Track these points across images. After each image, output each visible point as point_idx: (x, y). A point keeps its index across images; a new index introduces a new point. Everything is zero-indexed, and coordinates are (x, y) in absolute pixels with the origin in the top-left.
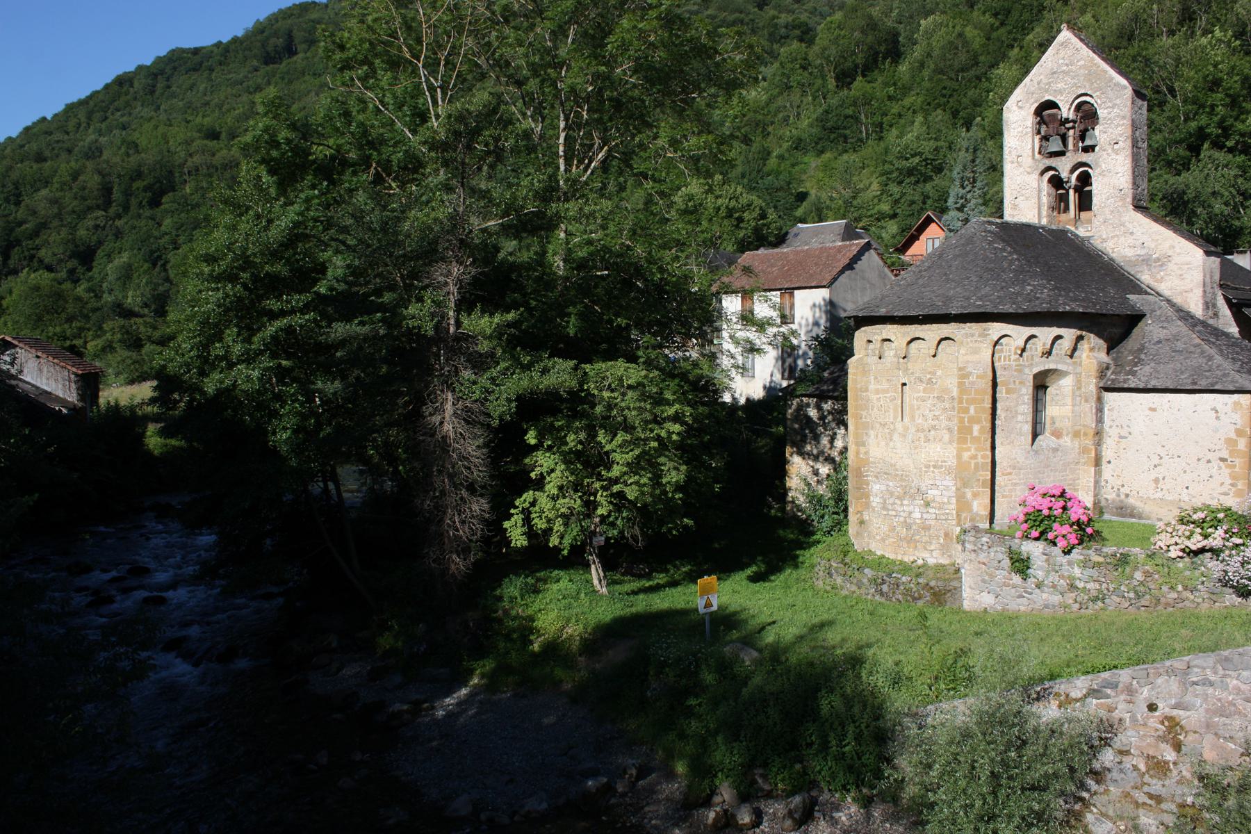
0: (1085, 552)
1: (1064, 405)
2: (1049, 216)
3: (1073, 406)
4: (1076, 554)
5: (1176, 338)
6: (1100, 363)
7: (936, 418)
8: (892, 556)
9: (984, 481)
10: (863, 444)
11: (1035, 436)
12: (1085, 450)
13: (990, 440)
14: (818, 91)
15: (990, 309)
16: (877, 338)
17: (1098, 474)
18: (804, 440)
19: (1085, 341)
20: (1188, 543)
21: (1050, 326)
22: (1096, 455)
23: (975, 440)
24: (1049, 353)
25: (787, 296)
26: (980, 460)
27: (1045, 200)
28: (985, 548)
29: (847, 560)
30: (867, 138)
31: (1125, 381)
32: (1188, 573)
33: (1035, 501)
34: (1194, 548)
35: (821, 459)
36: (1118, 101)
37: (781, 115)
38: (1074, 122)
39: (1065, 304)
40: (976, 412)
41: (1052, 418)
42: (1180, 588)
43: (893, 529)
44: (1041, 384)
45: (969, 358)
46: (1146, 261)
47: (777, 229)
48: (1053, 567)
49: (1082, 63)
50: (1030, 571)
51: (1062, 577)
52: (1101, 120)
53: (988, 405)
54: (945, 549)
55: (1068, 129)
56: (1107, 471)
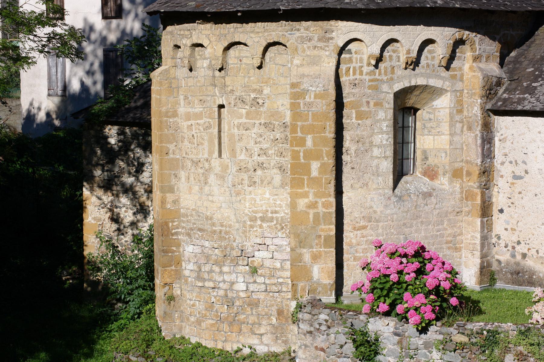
0: (445, 329)
1: (439, 134)
3: (451, 135)
4: (434, 333)
6: (487, 78)
7: (264, 152)
8: (209, 344)
9: (327, 238)
10: (171, 190)
11: (399, 173)
12: (468, 196)
13: (333, 182)
16: (186, 42)
17: (487, 226)
19: (466, 47)
22: (483, 202)
23: (314, 181)
26: (321, 209)
28: (323, 328)
29: (151, 352)
31: (520, 101)
33: (380, 262)
41: (424, 152)
43: (210, 306)
44: (405, 107)
45: (306, 70)
53: (330, 134)
54: (278, 332)
56: (499, 224)
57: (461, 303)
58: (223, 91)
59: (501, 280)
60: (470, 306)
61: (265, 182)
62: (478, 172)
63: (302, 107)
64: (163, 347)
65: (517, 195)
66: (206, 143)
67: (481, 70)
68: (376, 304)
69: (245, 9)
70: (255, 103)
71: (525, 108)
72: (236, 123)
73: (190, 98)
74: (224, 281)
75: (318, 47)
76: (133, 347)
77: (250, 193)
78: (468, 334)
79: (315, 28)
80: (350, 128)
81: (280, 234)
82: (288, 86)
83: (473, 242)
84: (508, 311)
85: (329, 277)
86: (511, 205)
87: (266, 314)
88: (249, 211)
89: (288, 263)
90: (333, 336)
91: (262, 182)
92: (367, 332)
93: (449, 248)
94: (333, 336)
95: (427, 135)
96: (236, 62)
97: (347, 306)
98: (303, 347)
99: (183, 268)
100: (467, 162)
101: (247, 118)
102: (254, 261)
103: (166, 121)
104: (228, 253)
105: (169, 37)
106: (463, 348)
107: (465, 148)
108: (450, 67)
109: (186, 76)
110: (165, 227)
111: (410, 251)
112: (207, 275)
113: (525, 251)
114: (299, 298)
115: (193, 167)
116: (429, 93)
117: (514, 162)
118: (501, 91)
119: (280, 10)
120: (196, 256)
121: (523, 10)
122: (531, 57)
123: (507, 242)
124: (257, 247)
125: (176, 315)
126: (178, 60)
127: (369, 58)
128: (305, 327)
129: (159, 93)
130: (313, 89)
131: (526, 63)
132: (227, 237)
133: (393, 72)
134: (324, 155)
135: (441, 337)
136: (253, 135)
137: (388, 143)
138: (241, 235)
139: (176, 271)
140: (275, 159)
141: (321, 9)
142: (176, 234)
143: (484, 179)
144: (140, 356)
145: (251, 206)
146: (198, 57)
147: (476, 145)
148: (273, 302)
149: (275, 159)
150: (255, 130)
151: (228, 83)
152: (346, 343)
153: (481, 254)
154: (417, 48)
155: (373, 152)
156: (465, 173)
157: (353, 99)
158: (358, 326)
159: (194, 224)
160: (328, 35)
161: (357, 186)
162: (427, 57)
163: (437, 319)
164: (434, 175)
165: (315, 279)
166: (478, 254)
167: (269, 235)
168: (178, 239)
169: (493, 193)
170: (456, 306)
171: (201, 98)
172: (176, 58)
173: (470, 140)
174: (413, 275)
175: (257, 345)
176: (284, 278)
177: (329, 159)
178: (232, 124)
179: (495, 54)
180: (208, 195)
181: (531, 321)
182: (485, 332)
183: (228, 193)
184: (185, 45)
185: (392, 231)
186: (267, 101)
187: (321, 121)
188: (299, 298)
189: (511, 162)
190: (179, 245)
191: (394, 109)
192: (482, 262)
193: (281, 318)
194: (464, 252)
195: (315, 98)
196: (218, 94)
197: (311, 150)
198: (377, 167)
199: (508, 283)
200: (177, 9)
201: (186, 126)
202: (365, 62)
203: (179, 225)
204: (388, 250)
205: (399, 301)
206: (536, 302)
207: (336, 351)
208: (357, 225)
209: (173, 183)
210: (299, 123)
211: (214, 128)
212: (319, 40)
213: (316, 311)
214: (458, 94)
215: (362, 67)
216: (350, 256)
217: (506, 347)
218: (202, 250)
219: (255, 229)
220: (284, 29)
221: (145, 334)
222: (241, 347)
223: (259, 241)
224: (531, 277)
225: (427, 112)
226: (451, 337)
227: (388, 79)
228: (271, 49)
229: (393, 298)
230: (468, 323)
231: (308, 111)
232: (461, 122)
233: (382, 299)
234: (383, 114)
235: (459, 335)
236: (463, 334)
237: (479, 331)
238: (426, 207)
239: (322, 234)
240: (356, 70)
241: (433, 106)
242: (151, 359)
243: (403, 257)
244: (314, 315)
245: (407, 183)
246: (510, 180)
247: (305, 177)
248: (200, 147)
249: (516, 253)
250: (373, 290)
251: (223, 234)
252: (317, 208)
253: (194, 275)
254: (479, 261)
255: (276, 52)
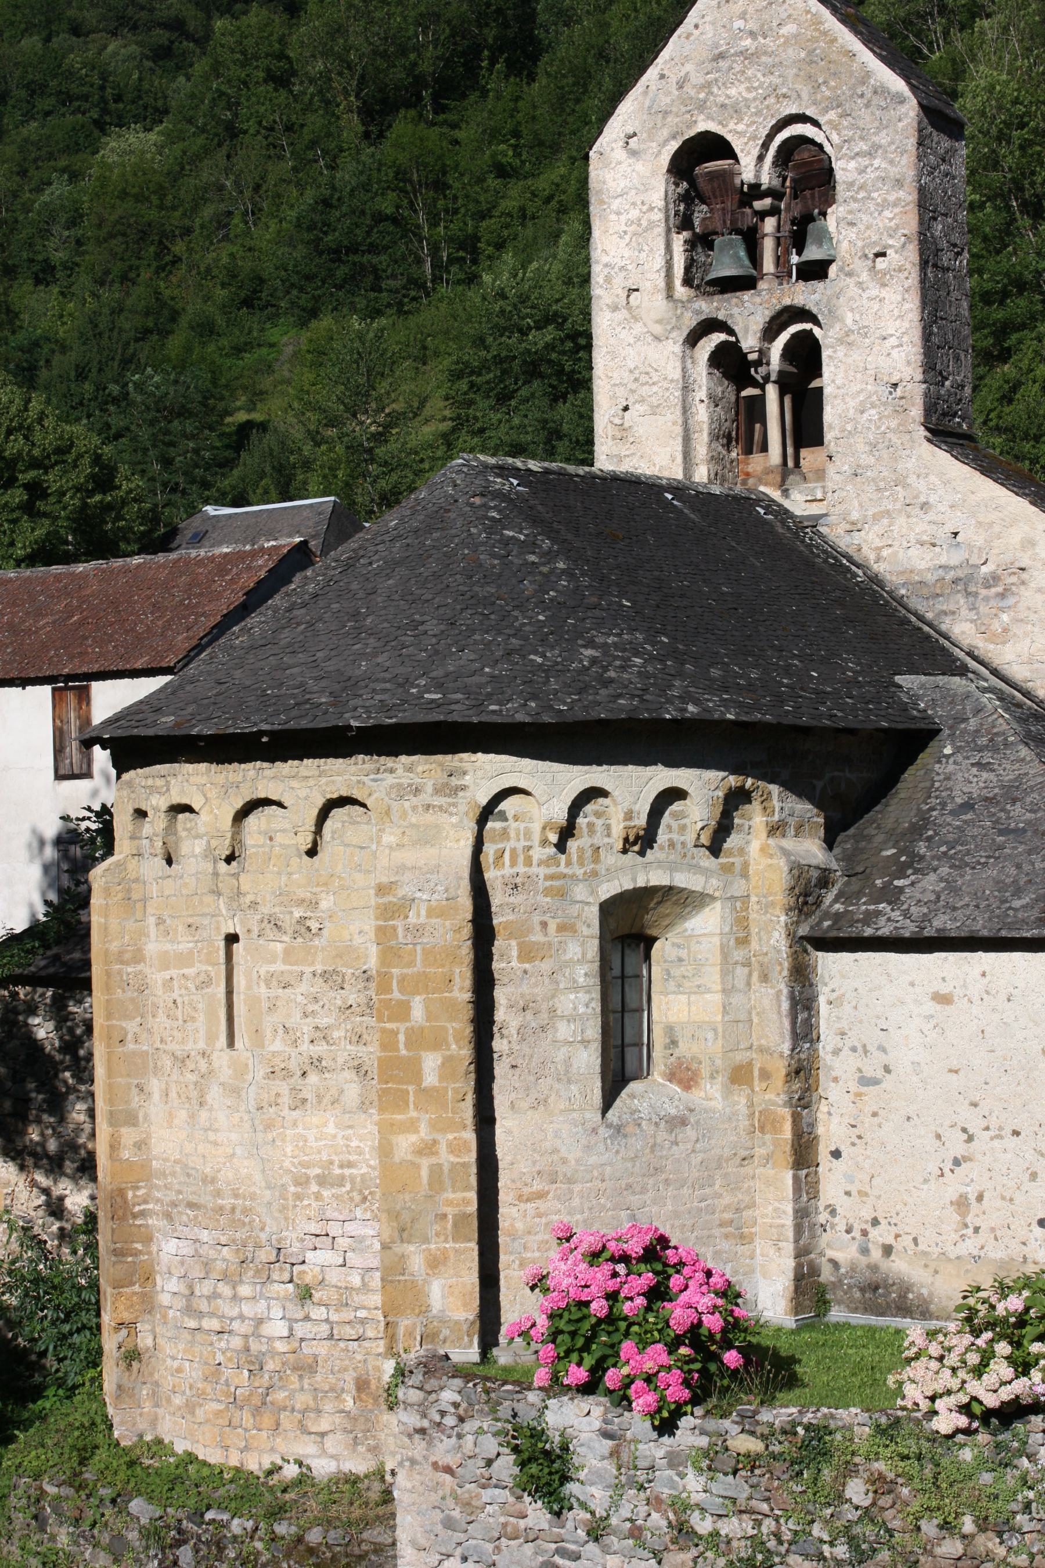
1: (700, 990)
2: (714, 459)
4: (689, 1433)
5: (1012, 793)
6: (798, 870)
7: (322, 1034)
8: (213, 1456)
9: (460, 1220)
10: (132, 1120)
12: (765, 1123)
13: (470, 1098)
14: (313, 144)
15: (461, 713)
17: (806, 1189)
18: (22, 1116)
19: (756, 806)
20: (976, 1388)
21: (645, 760)
24: (643, 841)
25: (71, 697)
26: (445, 1157)
27: (702, 414)
28: (450, 1421)
30: (436, 279)
31: (869, 918)
32: (987, 1478)
33: (568, 1274)
34: (991, 1401)
35: (69, 1166)
36: (883, 139)
37: (208, 212)
38: (771, 193)
39: (686, 697)
40: (429, 1016)
41: (670, 1030)
42: (968, 1525)
44: (629, 930)
45: (408, 856)
46: (963, 583)
47: (143, 518)
48: (631, 1476)
49: (790, 29)
50: (572, 1488)
51: (655, 1502)
52: (840, 188)
53: (462, 992)
54: (359, 1428)
55: (762, 215)
57: (748, 1362)
58: (235, 905)
59: (839, 1302)
60: (772, 1369)
61: (325, 1101)
62: (783, 1072)
63: (400, 935)
64: (115, 1464)
65: (868, 1120)
66: (201, 1018)
67: (785, 852)
68: (560, 1367)
69: (276, 727)
70: (303, 930)
71: (880, 933)
72: (262, 972)
73: (168, 921)
74: (242, 1317)
75: (434, 806)
76: (51, 1463)
77: (295, 1124)
78: (762, 1435)
79: (427, 767)
80: (506, 980)
81: (359, 1213)
82: (372, 892)
83: (779, 1221)
84: (854, 1374)
85: (465, 1305)
86: (857, 1141)
87: (332, 1389)
88: (293, 1164)
89: (378, 1275)
90: (470, 1439)
91: (319, 1097)
92: (543, 1430)
93: (727, 1236)
94: (470, 1439)
95: (674, 993)
96: (261, 841)
97: (505, 1369)
98: (407, 1464)
99: (158, 1288)
100: (761, 1050)
101: (285, 962)
102: (304, 1272)
103: (120, 972)
104: (250, 1256)
105: (125, 793)
106: (753, 1468)
107: (755, 1020)
108: (720, 850)
109: (160, 874)
110: (119, 1200)
111: (635, 1247)
112: (206, 1303)
113: (890, 1240)
114: (402, 1352)
115: (175, 1070)
116: (676, 903)
117: (860, 1049)
118: (829, 897)
119: (349, 727)
120: (182, 1263)
121: (869, 726)
122: (889, 826)
123: (851, 1221)
124: (310, 1241)
125: (145, 1392)
126: (145, 841)
127: (544, 828)
128: (413, 1420)
129: (106, 912)
130: (425, 897)
131: (880, 838)
132: (247, 1220)
133: (596, 860)
134: (451, 1039)
135: (703, 1441)
136: (300, 998)
137: (590, 1011)
138: (277, 1215)
139: (144, 1295)
140: (345, 1050)
141: (438, 724)
142: (143, 1214)
143: (797, 1085)
144: (64, 1483)
145: (297, 1153)
146: (184, 834)
147: (779, 1012)
148: (347, 1362)
149: (345, 1050)
150: (303, 987)
151: (244, 888)
152: (499, 1454)
153: (796, 1248)
154: (647, 808)
155: (556, 1030)
156: (756, 1073)
157: (511, 917)
158: (527, 1416)
159: (180, 1192)
160: (454, 781)
161: (524, 1105)
162: (669, 827)
163: (695, 1401)
164: (692, 1079)
165: (434, 1311)
166: (789, 1247)
167: (336, 1215)
168: (147, 1226)
169: (819, 1114)
170: (736, 1371)
171: (190, 921)
172: (140, 838)
173: (766, 1002)
174: (640, 1301)
175: (314, 1456)
176: (369, 1309)
177: (460, 1048)
178: (255, 976)
179: (815, 819)
180: (206, 1130)
181: (902, 1403)
182: (800, 1430)
183: (247, 1125)
184: (156, 809)
185: (602, 1201)
186: (327, 924)
187: (443, 966)
188: (402, 1352)
189: (854, 1049)
190: (148, 1239)
191: (602, 938)
192: (799, 1267)
193: (363, 1396)
194: (760, 1246)
195: (429, 915)
196: (224, 912)
197: (422, 1029)
198: (568, 1062)
199: (855, 1310)
200: (135, 732)
201: (160, 982)
202: (537, 838)
203: (148, 1194)
204: (584, 1247)
205: (611, 1361)
206: (913, 1359)
207: (478, 1472)
208: (526, 1190)
209: (134, 1105)
210: (395, 971)
211: (218, 985)
212: (437, 791)
213: (432, 1383)
214: (738, 904)
215: (530, 848)
216: (512, 1258)
217: (847, 1462)
218: (196, 1250)
219: (306, 1202)
220: (361, 770)
221: (77, 1433)
222: (279, 1462)
223: (314, 1228)
224: (903, 1296)
225: (674, 944)
226: (725, 1441)
227: (585, 873)
228: (336, 813)
229: (598, 1355)
230: (763, 1410)
231: (415, 944)
232: (747, 964)
233: (575, 1357)
234: (578, 950)
235: (743, 1436)
236: (752, 1433)
237: (788, 1427)
238: (675, 1148)
239: (450, 1211)
240: (517, 856)
241: (686, 930)
242: (87, 1491)
243: (619, 1261)
244: (430, 1393)
245: (632, 1096)
246: (854, 1087)
247: (411, 1088)
248: (190, 1026)
249: (870, 1245)
250: (555, 1335)
251: (238, 1215)
252: (437, 1153)
253: (180, 1303)
254: (791, 1263)
255: (346, 818)
